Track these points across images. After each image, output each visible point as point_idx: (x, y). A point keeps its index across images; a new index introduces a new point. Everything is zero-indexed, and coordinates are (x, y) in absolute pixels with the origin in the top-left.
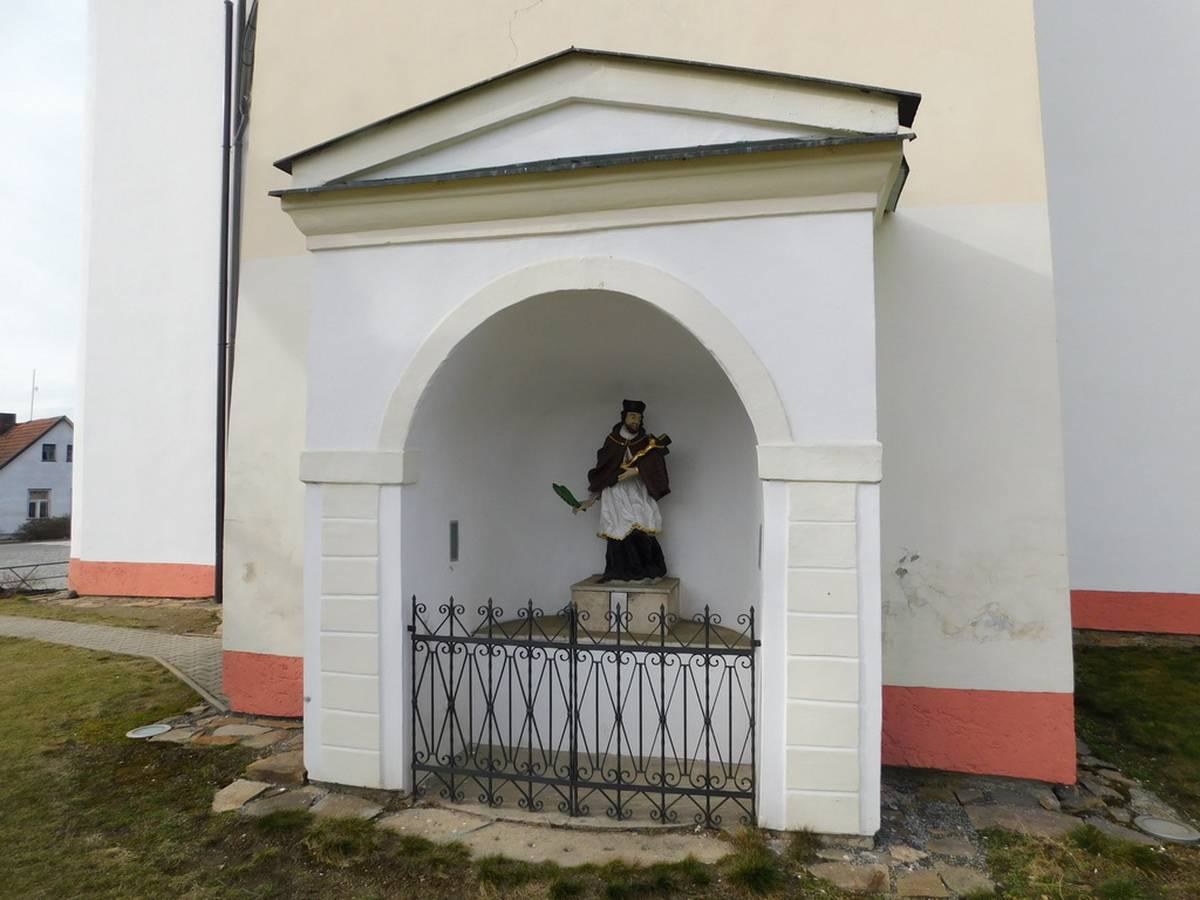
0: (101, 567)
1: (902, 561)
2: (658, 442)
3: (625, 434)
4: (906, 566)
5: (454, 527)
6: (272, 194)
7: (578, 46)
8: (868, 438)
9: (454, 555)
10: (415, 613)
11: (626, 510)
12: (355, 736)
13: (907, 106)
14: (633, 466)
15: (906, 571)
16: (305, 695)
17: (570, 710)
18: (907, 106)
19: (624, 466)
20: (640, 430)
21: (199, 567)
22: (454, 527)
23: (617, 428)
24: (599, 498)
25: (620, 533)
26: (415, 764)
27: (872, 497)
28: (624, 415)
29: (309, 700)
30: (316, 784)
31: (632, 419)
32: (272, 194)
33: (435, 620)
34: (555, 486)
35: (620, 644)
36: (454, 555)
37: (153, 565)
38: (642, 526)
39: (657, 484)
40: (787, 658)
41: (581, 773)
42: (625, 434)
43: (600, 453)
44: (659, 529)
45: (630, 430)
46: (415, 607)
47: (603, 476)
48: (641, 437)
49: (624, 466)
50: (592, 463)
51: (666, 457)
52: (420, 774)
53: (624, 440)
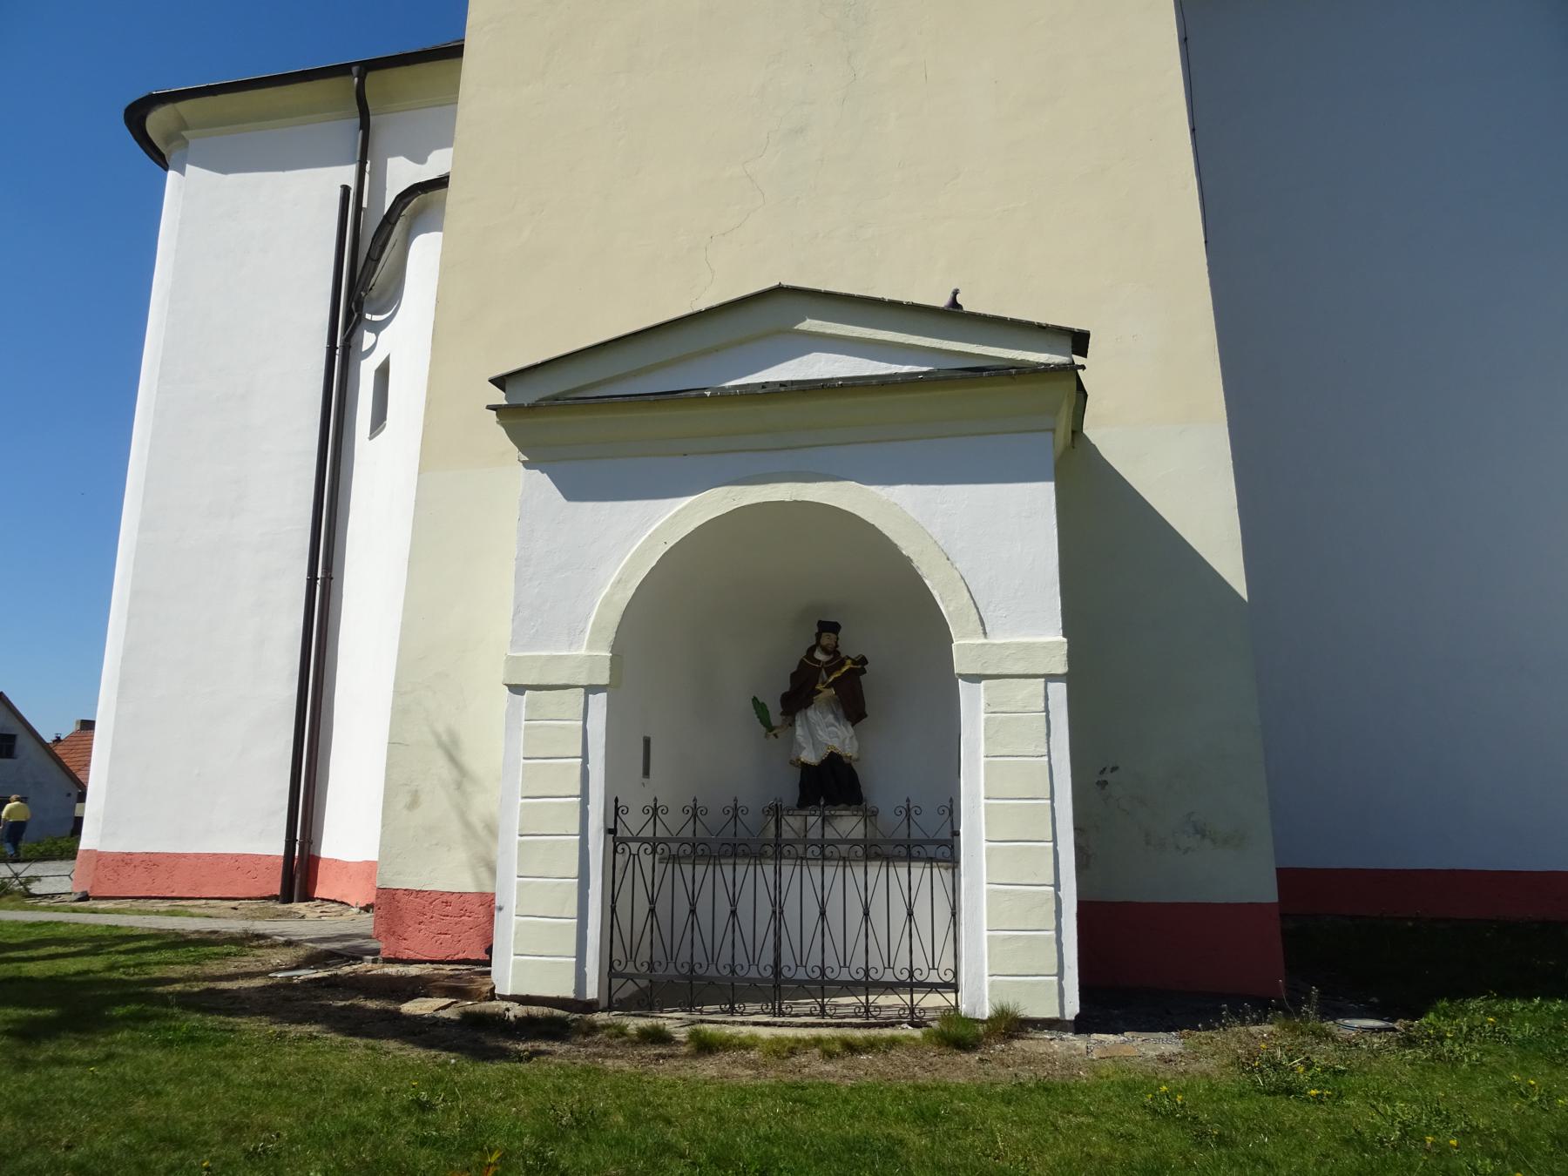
0: (126, 860)
1: (1102, 772)
2: (854, 662)
3: (819, 655)
4: (1108, 776)
5: (647, 742)
6: (489, 407)
7: (785, 283)
8: (1055, 637)
9: (646, 773)
10: (617, 814)
11: (822, 734)
12: (538, 957)
13: (1080, 341)
14: (828, 687)
15: (1106, 783)
16: (497, 904)
17: (774, 905)
18: (1080, 341)
19: (819, 687)
20: (834, 652)
21: (259, 857)
22: (647, 742)
23: (811, 650)
24: (792, 724)
25: (810, 756)
26: (611, 972)
27: (1059, 691)
28: (818, 636)
29: (500, 909)
30: (504, 998)
31: (827, 639)
32: (489, 407)
33: (634, 822)
34: (755, 699)
35: (826, 851)
36: (646, 773)
37: (198, 856)
38: (839, 750)
39: (853, 708)
40: (985, 844)
41: (785, 971)
42: (819, 655)
43: (793, 676)
44: (855, 756)
45: (825, 651)
46: (617, 809)
47: (798, 697)
48: (837, 659)
49: (819, 687)
50: (786, 687)
51: (862, 678)
52: (616, 982)
53: (819, 662)
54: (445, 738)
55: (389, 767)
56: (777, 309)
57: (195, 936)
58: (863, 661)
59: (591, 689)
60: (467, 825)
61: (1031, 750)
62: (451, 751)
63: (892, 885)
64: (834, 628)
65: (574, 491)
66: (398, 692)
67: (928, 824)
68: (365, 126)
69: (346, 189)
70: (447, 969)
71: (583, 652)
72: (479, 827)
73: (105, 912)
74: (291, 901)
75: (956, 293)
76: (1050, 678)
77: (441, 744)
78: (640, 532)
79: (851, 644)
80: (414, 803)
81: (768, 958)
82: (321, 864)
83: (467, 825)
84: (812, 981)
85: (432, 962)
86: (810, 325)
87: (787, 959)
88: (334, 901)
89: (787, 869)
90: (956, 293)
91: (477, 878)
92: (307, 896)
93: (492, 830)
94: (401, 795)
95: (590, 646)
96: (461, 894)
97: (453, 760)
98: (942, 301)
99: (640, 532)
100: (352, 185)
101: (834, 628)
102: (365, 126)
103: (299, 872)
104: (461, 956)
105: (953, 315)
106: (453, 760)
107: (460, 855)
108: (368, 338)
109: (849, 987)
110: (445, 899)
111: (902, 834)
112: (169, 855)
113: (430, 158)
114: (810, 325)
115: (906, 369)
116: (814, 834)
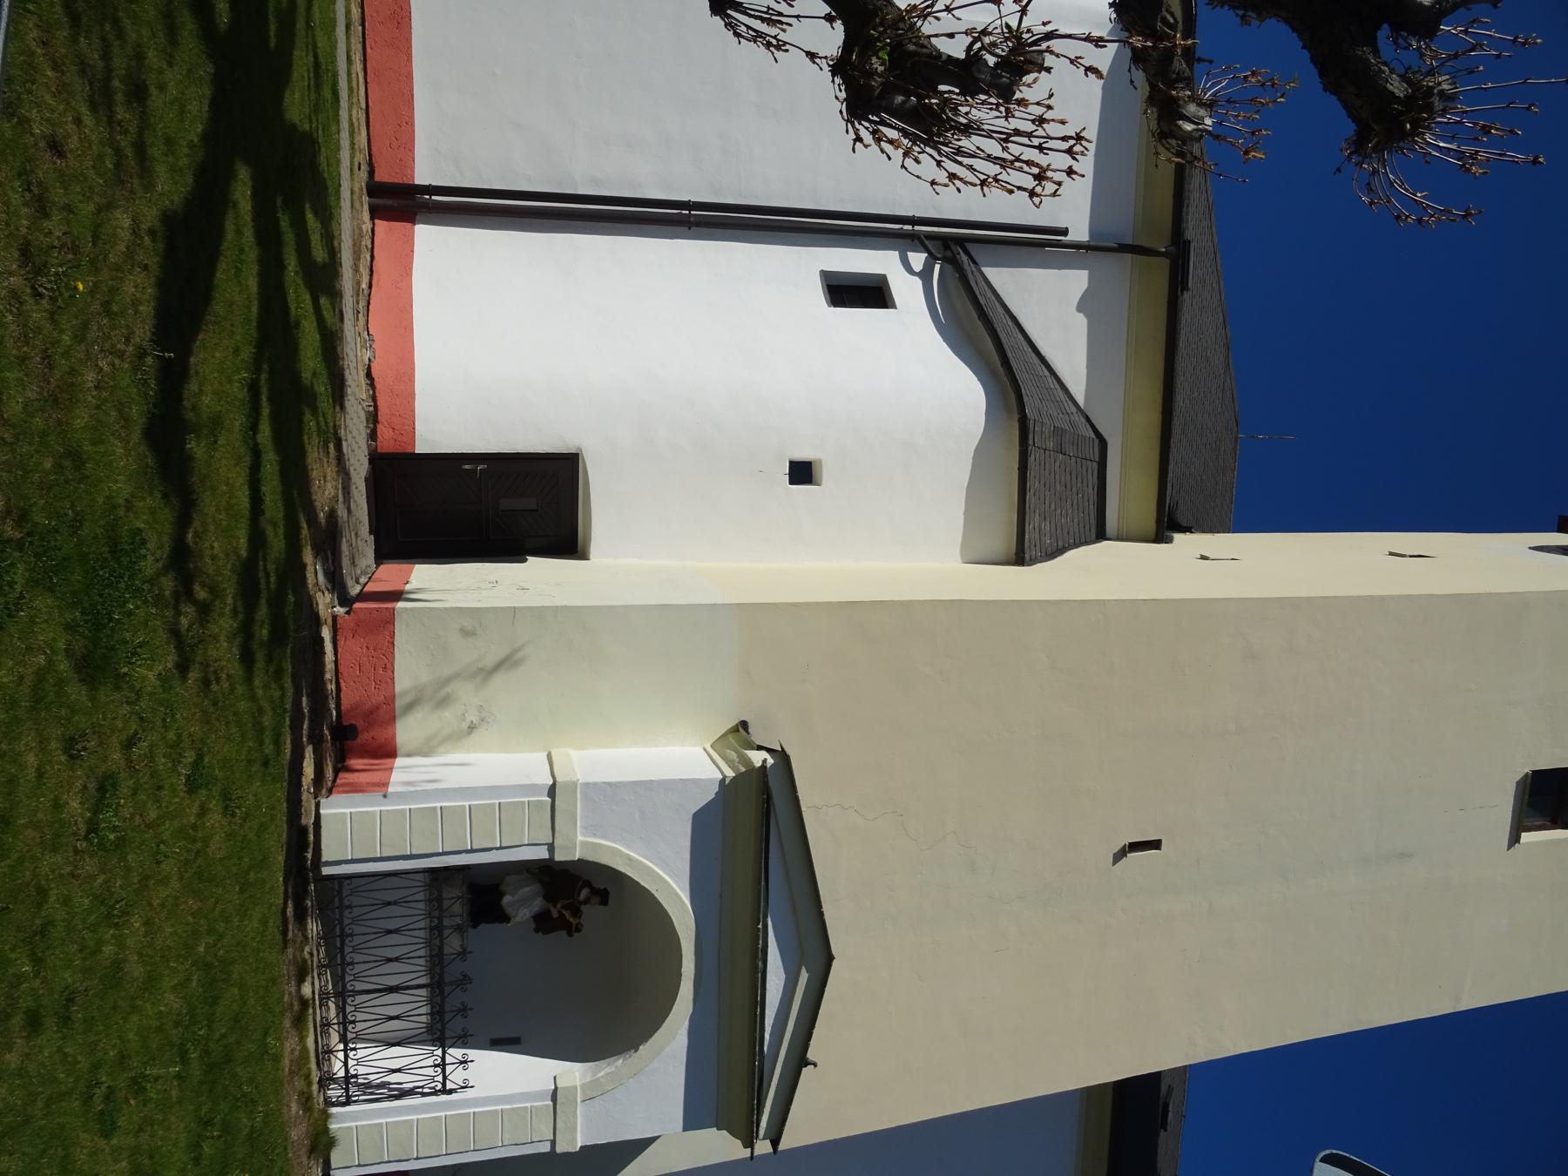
21: (412, 150)
23: (588, 884)
27: (546, 1148)
30: (318, 805)
39: (543, 922)
54: (520, 655)
55: (495, 609)
56: (815, 955)
57: (336, 243)
58: (578, 930)
59: (551, 847)
60: (449, 680)
61: (506, 1136)
62: (508, 662)
63: (415, 1008)
64: (604, 902)
65: (701, 820)
66: (556, 610)
67: (455, 1026)
68: (1123, 248)
69: (1065, 232)
70: (331, 687)
71: (580, 838)
72: (443, 693)
73: (356, 269)
74: (370, 194)
75: (815, 1065)
76: (553, 1143)
77: (515, 652)
78: (665, 872)
79: (592, 914)
80: (466, 633)
81: (359, 986)
82: (408, 225)
83: (449, 680)
84: (344, 986)
85: (336, 662)
86: (804, 976)
87: (359, 999)
88: (372, 257)
89: (423, 992)
90: (815, 1065)
91: (404, 693)
92: (375, 213)
93: (443, 702)
94: (472, 622)
95: (583, 844)
96: (393, 679)
97: (497, 667)
98: (811, 1055)
99: (665, 872)
100: (1070, 238)
101: (604, 902)
102: (1123, 248)
103: (404, 202)
104: (343, 684)
105: (800, 1061)
106: (497, 667)
107: (425, 677)
108: (918, 259)
109: (341, 1010)
110: (389, 667)
111: (447, 978)
112: (409, 40)
113: (1081, 321)
114: (804, 976)
115: (767, 1036)
116: (446, 922)
